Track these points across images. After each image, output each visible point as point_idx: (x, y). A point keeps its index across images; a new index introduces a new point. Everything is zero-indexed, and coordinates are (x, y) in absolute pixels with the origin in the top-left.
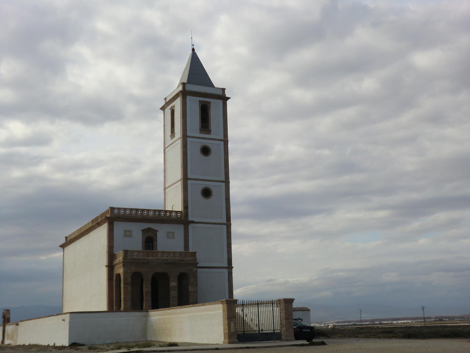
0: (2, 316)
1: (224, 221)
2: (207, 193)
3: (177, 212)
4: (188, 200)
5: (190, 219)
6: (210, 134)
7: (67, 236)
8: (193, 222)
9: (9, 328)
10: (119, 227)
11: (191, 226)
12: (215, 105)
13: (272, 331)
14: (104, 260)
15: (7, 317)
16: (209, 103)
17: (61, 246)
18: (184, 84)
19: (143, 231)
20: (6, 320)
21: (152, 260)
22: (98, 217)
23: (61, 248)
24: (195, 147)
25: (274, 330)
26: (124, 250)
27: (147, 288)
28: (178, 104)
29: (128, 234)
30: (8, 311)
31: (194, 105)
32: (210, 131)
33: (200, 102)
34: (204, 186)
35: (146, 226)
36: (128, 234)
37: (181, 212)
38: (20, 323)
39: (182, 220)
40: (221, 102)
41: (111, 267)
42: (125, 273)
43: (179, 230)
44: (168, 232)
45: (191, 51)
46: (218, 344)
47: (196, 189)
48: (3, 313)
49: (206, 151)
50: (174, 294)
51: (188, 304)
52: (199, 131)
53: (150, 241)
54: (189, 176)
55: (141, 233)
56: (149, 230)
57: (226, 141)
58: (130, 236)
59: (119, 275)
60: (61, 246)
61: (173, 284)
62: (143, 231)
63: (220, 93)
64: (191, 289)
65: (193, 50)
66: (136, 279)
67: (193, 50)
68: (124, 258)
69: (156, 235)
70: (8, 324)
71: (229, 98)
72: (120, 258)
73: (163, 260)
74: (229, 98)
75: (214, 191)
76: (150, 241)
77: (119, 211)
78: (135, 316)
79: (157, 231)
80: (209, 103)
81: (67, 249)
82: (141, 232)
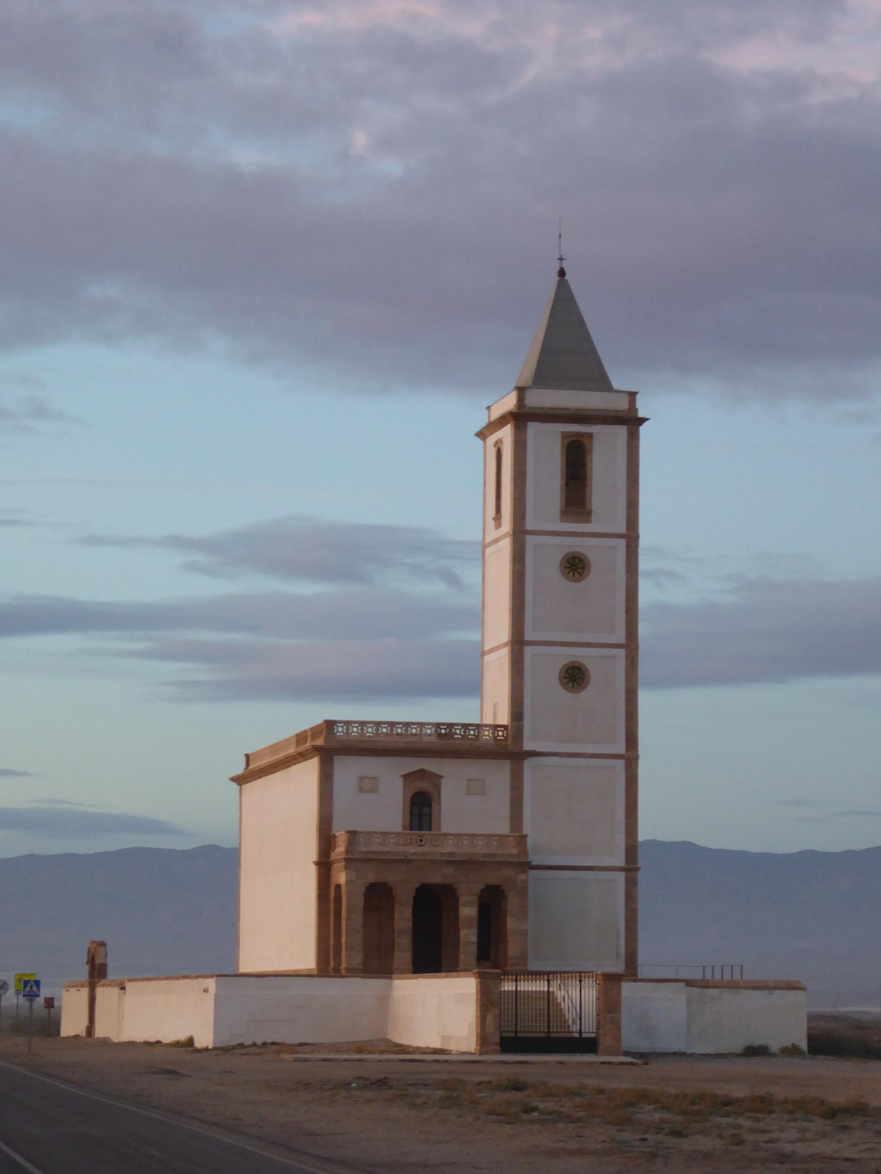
0: (85, 960)
1: (620, 748)
2: (574, 676)
3: (495, 727)
4: (522, 697)
5: (528, 746)
6: (588, 521)
7: (249, 752)
8: (534, 754)
9: (105, 995)
10: (347, 771)
11: (529, 765)
12: (606, 444)
13: (512, 1035)
14: (311, 852)
15: (98, 961)
16: (590, 436)
17: (233, 779)
18: (521, 391)
19: (405, 777)
20: (97, 972)
21: (413, 854)
22: (305, 732)
23: (235, 784)
24: (546, 556)
25: (516, 1032)
26: (348, 832)
27: (403, 917)
28: (506, 433)
29: (368, 786)
30: (102, 944)
31: (546, 442)
32: (589, 513)
33: (565, 435)
34: (566, 661)
35: (413, 764)
36: (368, 786)
37: (505, 727)
38: (129, 986)
39: (507, 749)
40: (622, 431)
41: (324, 866)
42: (348, 882)
43: (498, 776)
44: (469, 780)
45: (556, 279)
46: (277, 1047)
47: (545, 667)
48: (89, 949)
49: (575, 566)
50: (469, 936)
51: (456, 971)
52: (558, 515)
53: (421, 807)
54: (529, 636)
55: (400, 783)
56: (421, 774)
57: (631, 538)
58: (374, 790)
59: (338, 887)
60: (233, 779)
61: (468, 911)
62: (405, 777)
63: (622, 405)
64: (511, 924)
65: (562, 273)
66: (378, 897)
67: (562, 273)
68: (348, 851)
69: (438, 788)
70: (103, 982)
71: (643, 420)
72: (340, 849)
73: (442, 854)
74: (643, 420)
75: (595, 673)
76: (421, 807)
77: (348, 729)
78: (369, 987)
79: (441, 777)
80: (590, 436)
81: (246, 787)
82: (402, 779)
